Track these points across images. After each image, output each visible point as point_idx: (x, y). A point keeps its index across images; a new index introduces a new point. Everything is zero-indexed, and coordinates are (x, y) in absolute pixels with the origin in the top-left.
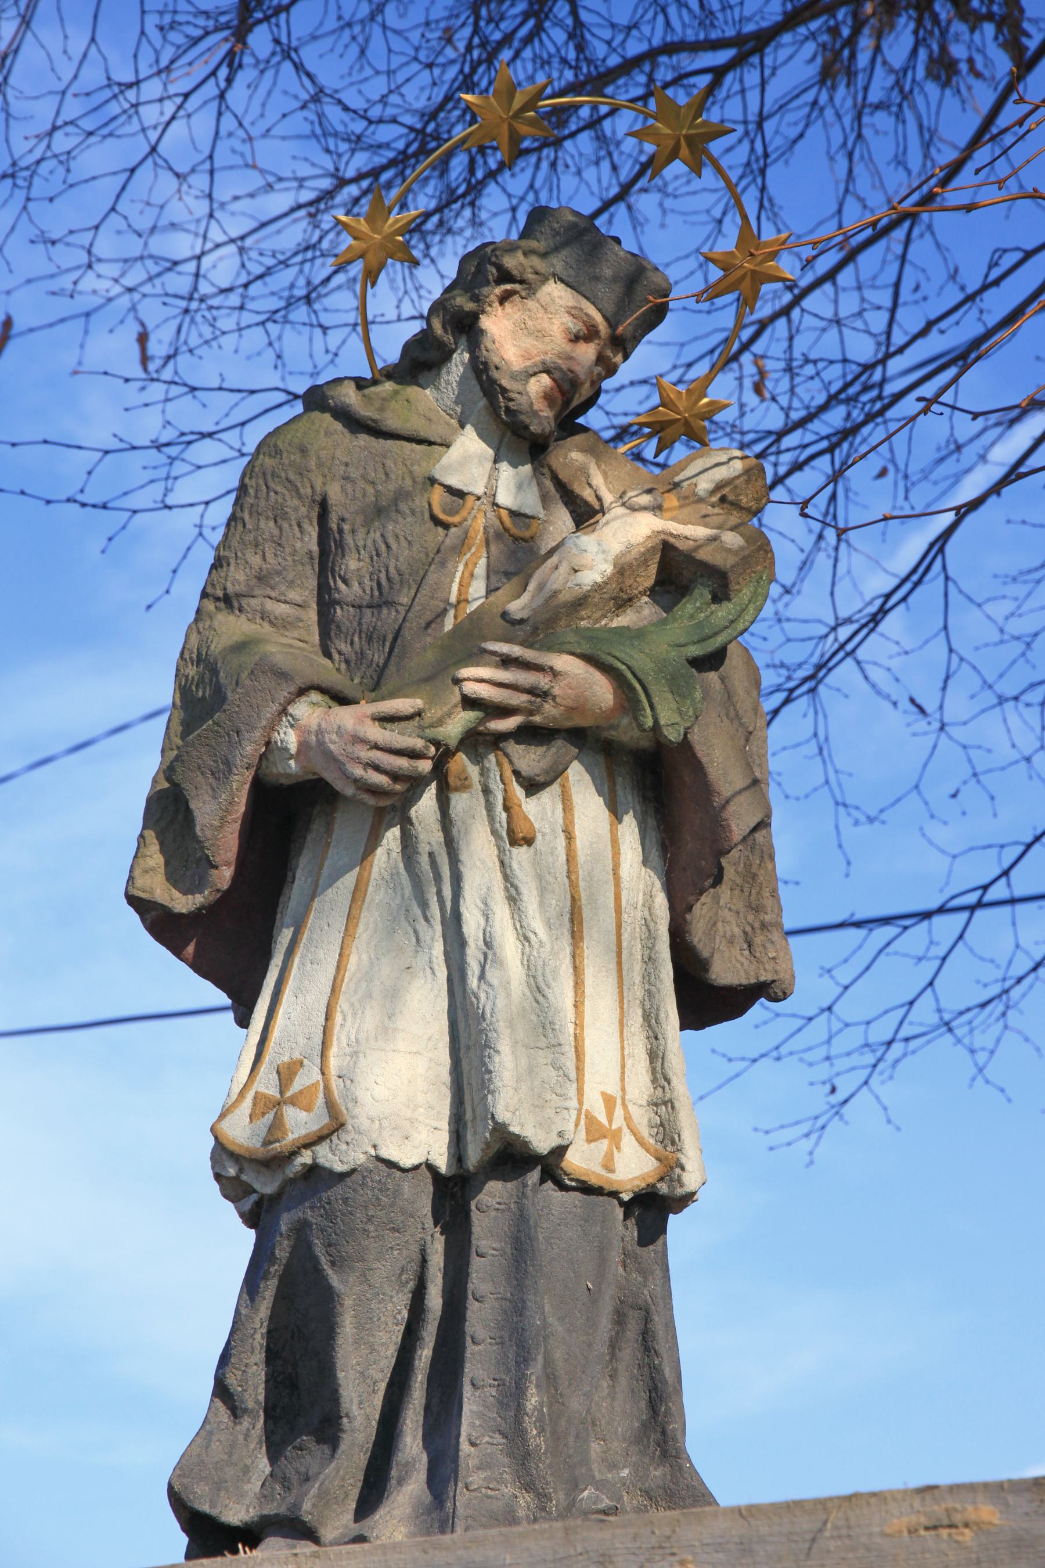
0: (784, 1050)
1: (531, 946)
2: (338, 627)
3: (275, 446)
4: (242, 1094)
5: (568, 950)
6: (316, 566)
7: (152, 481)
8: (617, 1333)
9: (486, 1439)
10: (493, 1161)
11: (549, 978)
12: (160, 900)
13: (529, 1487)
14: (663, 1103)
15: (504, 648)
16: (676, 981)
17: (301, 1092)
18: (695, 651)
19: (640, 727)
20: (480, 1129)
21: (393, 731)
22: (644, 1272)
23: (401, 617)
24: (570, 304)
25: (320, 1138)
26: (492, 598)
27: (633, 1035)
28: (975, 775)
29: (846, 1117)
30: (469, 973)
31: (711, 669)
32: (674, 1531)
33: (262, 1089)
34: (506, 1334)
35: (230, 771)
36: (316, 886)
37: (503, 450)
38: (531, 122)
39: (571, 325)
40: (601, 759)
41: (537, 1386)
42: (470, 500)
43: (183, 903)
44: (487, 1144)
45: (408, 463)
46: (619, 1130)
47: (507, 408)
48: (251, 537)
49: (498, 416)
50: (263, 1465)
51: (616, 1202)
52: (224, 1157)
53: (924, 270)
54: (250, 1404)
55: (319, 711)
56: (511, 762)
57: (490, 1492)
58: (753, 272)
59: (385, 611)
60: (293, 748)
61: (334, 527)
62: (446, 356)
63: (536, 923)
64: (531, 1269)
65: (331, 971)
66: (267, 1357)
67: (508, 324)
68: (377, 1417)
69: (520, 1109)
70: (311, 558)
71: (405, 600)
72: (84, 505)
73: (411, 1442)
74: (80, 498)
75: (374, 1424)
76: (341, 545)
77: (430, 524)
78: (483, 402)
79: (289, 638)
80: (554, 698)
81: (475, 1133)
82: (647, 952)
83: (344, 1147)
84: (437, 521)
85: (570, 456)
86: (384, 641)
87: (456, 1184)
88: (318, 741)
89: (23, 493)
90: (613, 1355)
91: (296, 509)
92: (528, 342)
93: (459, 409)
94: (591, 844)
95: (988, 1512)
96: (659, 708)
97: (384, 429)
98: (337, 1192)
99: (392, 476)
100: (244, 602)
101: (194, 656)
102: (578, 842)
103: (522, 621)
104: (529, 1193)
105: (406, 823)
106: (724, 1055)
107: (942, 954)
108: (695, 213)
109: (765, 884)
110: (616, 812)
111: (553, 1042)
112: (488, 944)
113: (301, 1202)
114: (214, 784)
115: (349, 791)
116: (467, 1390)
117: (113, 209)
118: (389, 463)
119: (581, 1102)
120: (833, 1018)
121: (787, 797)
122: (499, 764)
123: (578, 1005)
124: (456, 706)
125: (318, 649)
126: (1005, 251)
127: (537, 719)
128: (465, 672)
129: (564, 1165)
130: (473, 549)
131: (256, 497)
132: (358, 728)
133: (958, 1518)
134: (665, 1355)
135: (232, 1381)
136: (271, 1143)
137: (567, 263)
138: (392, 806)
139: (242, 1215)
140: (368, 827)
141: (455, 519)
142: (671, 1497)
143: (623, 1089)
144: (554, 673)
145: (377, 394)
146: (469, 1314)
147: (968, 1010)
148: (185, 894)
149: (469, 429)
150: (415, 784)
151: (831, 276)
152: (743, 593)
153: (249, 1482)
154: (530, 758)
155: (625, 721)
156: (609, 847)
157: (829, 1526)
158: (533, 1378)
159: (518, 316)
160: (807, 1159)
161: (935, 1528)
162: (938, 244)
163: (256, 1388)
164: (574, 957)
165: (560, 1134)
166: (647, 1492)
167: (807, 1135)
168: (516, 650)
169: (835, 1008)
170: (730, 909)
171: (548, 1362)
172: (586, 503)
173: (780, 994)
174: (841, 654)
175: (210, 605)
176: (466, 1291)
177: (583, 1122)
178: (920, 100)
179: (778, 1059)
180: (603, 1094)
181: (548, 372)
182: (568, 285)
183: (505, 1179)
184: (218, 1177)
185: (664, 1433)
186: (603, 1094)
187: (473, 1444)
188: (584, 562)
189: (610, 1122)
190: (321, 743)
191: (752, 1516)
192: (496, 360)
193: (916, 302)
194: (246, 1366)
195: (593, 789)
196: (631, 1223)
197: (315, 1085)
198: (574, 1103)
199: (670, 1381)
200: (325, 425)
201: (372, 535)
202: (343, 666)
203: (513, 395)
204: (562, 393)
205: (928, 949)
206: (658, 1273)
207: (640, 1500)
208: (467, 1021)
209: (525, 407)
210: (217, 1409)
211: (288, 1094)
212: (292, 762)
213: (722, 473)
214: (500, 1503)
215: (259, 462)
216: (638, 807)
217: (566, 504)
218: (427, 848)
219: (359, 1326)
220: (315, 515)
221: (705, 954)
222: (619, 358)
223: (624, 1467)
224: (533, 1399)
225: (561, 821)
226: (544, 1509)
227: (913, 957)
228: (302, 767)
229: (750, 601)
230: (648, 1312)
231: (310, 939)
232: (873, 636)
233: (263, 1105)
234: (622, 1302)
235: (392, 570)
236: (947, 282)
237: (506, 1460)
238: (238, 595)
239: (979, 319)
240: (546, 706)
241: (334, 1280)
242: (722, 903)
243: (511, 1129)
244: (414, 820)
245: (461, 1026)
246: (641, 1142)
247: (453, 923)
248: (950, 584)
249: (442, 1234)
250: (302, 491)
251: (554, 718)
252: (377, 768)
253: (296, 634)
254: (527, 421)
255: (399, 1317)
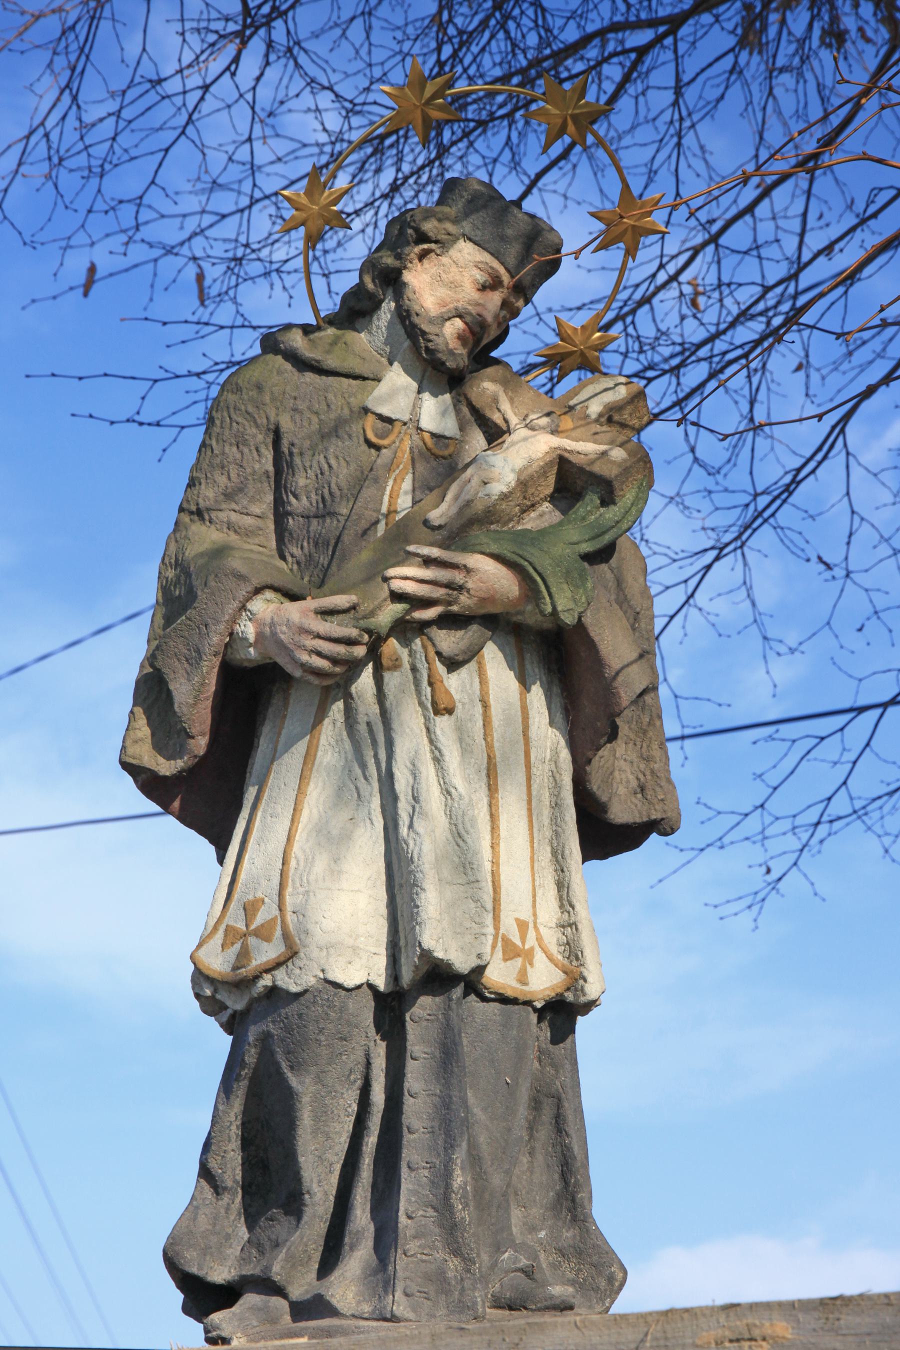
0: (726, 840)
1: (452, 799)
2: (291, 534)
3: (237, 384)
4: (215, 928)
5: (485, 800)
6: (272, 483)
7: (195, 402)
8: (535, 1117)
9: (421, 1213)
10: (421, 983)
11: (468, 825)
12: (148, 766)
13: (456, 1252)
14: (569, 925)
15: (426, 551)
16: (579, 822)
17: (262, 925)
18: (586, 548)
19: (542, 612)
20: (410, 954)
21: (332, 622)
22: (556, 1066)
23: (341, 525)
24: (477, 259)
25: (278, 964)
26: (416, 508)
27: (544, 868)
28: (876, 612)
29: (781, 891)
30: (401, 823)
31: (601, 562)
32: (521, 1339)
33: (232, 923)
34: (436, 1124)
35: (201, 658)
36: (275, 750)
37: (425, 382)
38: (440, 108)
39: (478, 277)
40: (512, 640)
41: (462, 1168)
42: (398, 425)
43: (166, 767)
44: (416, 967)
45: (346, 395)
46: (532, 949)
47: (427, 348)
48: (218, 460)
49: (420, 354)
50: (244, 1233)
51: (530, 1009)
52: (202, 979)
53: (826, 202)
54: (229, 1183)
55: (272, 607)
56: (434, 645)
57: (424, 1257)
58: (633, 226)
59: (328, 520)
60: (252, 638)
61: (286, 450)
62: (377, 305)
63: (458, 781)
64: (456, 1070)
65: (287, 823)
66: (242, 1144)
67: (426, 277)
68: (334, 1192)
69: (441, 937)
70: (268, 477)
71: (345, 511)
72: (141, 424)
73: (361, 1216)
74: (137, 418)
75: (332, 1198)
76: (291, 465)
77: (364, 447)
78: (407, 343)
79: (251, 545)
80: (468, 591)
81: (407, 956)
82: (554, 800)
83: (298, 971)
84: (370, 444)
85: (485, 386)
86: (328, 545)
87: (394, 999)
88: (271, 632)
89: (91, 416)
90: (531, 1136)
91: (254, 436)
92: (443, 292)
93: (388, 349)
94: (504, 710)
95: (782, 1328)
96: (556, 596)
97: (325, 367)
98: (291, 1010)
99: (333, 407)
100: (213, 515)
101: (173, 561)
102: (493, 709)
103: (440, 527)
104: (454, 1006)
105: (348, 697)
106: (676, 847)
107: (853, 758)
108: (636, 166)
109: (654, 738)
110: (525, 683)
111: (472, 879)
112: (416, 799)
113: (265, 1017)
114: (189, 669)
115: (297, 673)
116: (404, 1171)
117: (153, 182)
118: (331, 396)
119: (497, 928)
120: (765, 813)
121: (720, 635)
122: (424, 647)
123: (494, 846)
124: (385, 600)
125: (275, 553)
126: (881, 189)
127: (455, 608)
128: (391, 572)
129: (484, 980)
130: (401, 467)
131: (222, 427)
132: (304, 620)
133: (756, 1333)
134: (574, 1136)
135: (213, 1164)
136: (238, 968)
137: (474, 225)
138: (336, 683)
139: (222, 1026)
140: (317, 702)
141: (385, 442)
142: (580, 1254)
143: (535, 915)
144: (468, 570)
145: (321, 338)
146: (405, 1107)
147: (879, 797)
148: (168, 759)
149: (396, 364)
150: (353, 667)
151: (750, 209)
152: (627, 496)
153: (230, 1247)
154: (449, 641)
155: (529, 608)
156: (519, 713)
157: (649, 1337)
158: (459, 1161)
159: (434, 270)
160: (753, 925)
161: (738, 1340)
162: (836, 180)
163: (234, 1170)
164: (490, 806)
165: (479, 956)
166: (560, 1251)
167: (749, 907)
168: (435, 552)
169: (766, 806)
170: (625, 760)
171: (473, 1146)
172: (496, 425)
173: (669, 829)
174: (760, 521)
175: (186, 518)
176: (402, 1089)
177: (500, 944)
178: (815, 63)
179: (722, 847)
180: (517, 920)
181: (460, 316)
182: (475, 243)
183: (434, 994)
184: (198, 996)
185: (573, 1200)
186: (517, 920)
187: (410, 1217)
188: (491, 476)
189: (523, 943)
190: (274, 634)
191: (585, 1327)
192: (416, 308)
193: (821, 228)
194: (225, 1152)
195: (505, 665)
196: (545, 1025)
197: (274, 920)
198: (490, 930)
199: (579, 1157)
200: (277, 366)
201: (316, 457)
202: (295, 567)
203: (431, 337)
204: (472, 332)
205: (842, 754)
206: (568, 1067)
207: (554, 1257)
208: (399, 862)
209: (442, 347)
210: (202, 1188)
211: (252, 927)
212: (251, 650)
213: (610, 397)
214: (433, 1267)
215: (224, 397)
216: (544, 679)
217: (479, 426)
218: (366, 719)
219: (316, 1118)
220: (270, 440)
221: (604, 798)
222: (521, 303)
223: (541, 1229)
224: (459, 1179)
225: (478, 692)
226: (469, 1271)
227: (829, 762)
228: (260, 653)
229: (632, 504)
230: (559, 1099)
231: (270, 796)
232: (785, 506)
233: (231, 936)
234: (538, 1091)
235: (333, 486)
236: (845, 211)
237: (437, 1230)
238: (208, 510)
239: (861, 247)
240: (462, 597)
241: (293, 1080)
242: (618, 755)
243: (436, 954)
244: (354, 695)
245: (395, 867)
246: (550, 958)
247: (387, 780)
248: (851, 458)
249: (382, 1039)
250: (259, 421)
251: (469, 607)
252: (319, 654)
253: (257, 541)
254: (444, 358)
255: (350, 1110)
